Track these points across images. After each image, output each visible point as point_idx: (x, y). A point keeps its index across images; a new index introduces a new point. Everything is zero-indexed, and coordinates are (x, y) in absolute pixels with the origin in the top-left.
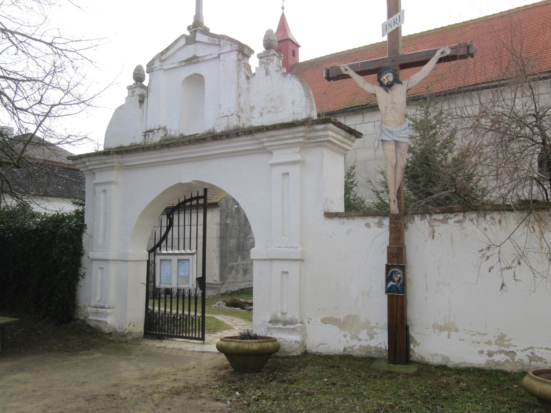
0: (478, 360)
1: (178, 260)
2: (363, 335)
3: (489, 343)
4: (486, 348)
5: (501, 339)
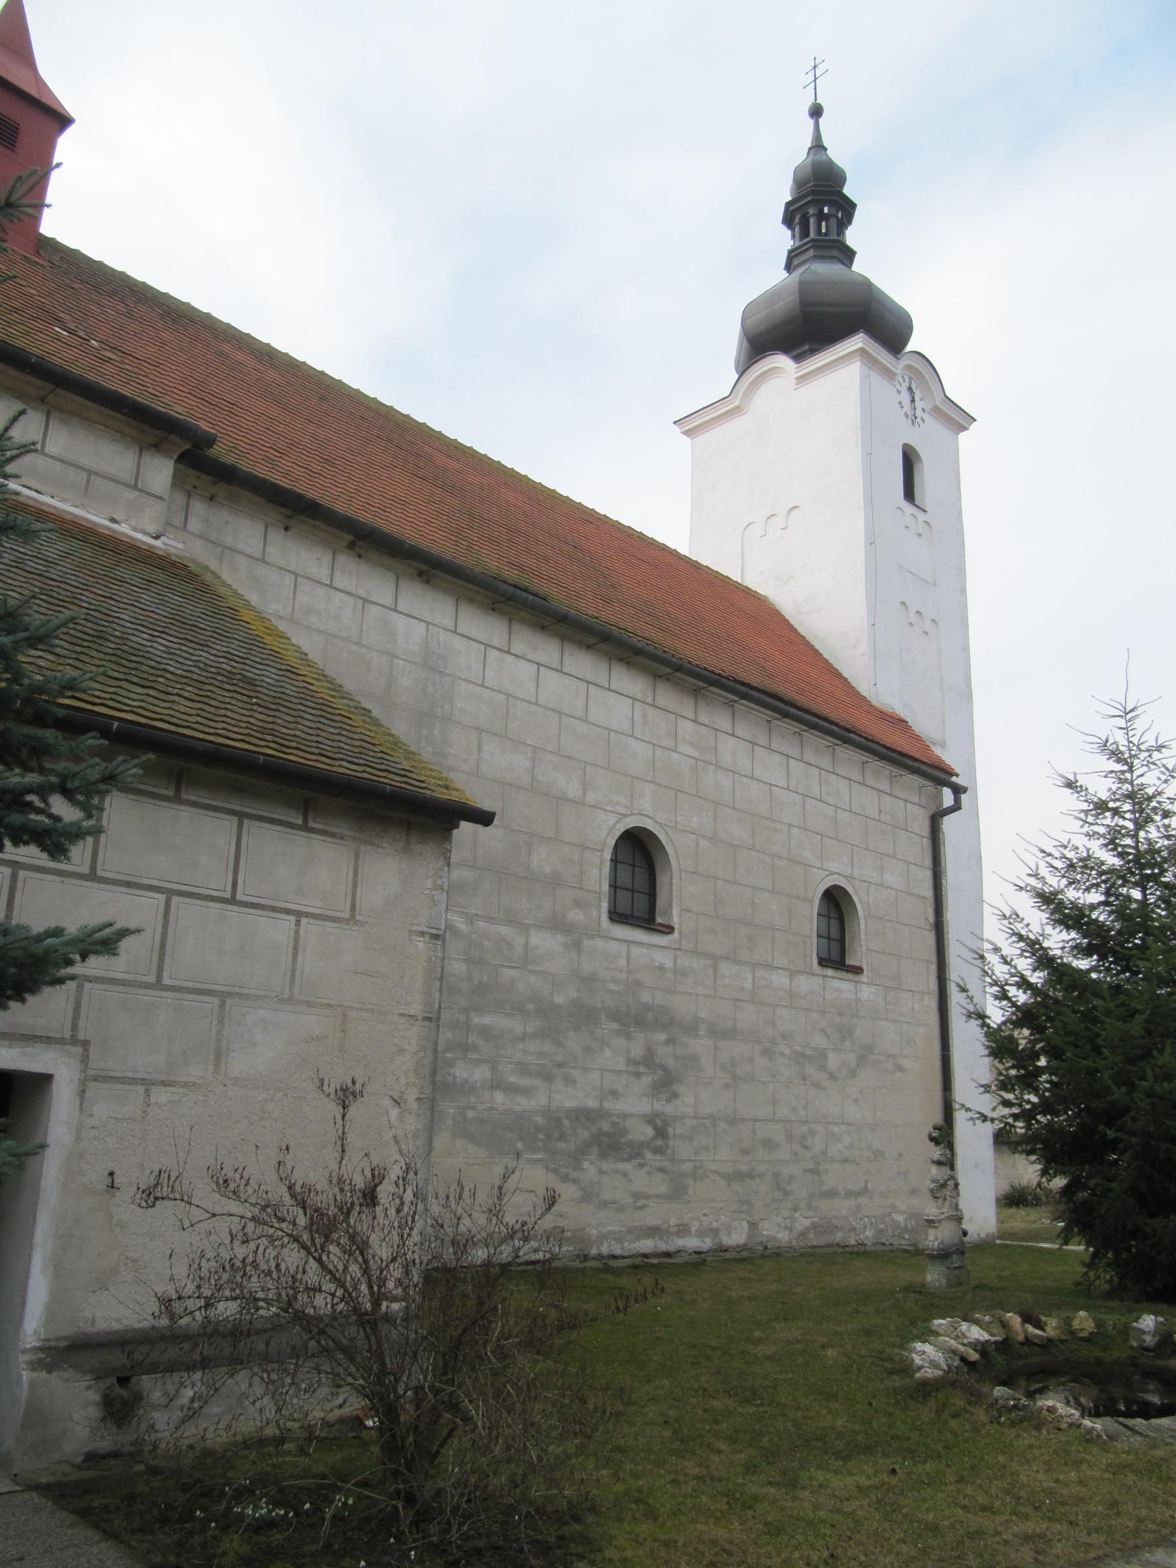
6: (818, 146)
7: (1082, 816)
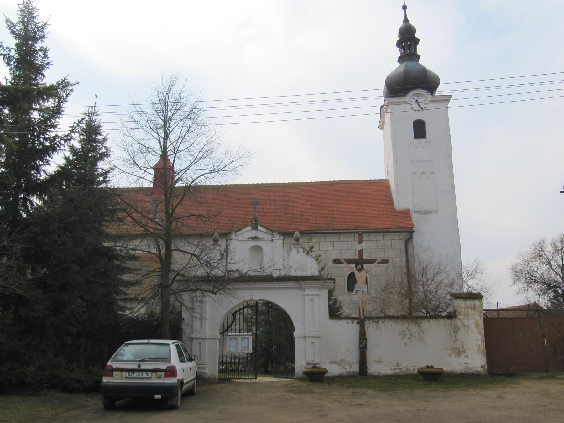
0: (390, 372)
2: (348, 367)
3: (394, 366)
4: (393, 368)
5: (398, 364)
6: (406, 20)
7: (161, 85)
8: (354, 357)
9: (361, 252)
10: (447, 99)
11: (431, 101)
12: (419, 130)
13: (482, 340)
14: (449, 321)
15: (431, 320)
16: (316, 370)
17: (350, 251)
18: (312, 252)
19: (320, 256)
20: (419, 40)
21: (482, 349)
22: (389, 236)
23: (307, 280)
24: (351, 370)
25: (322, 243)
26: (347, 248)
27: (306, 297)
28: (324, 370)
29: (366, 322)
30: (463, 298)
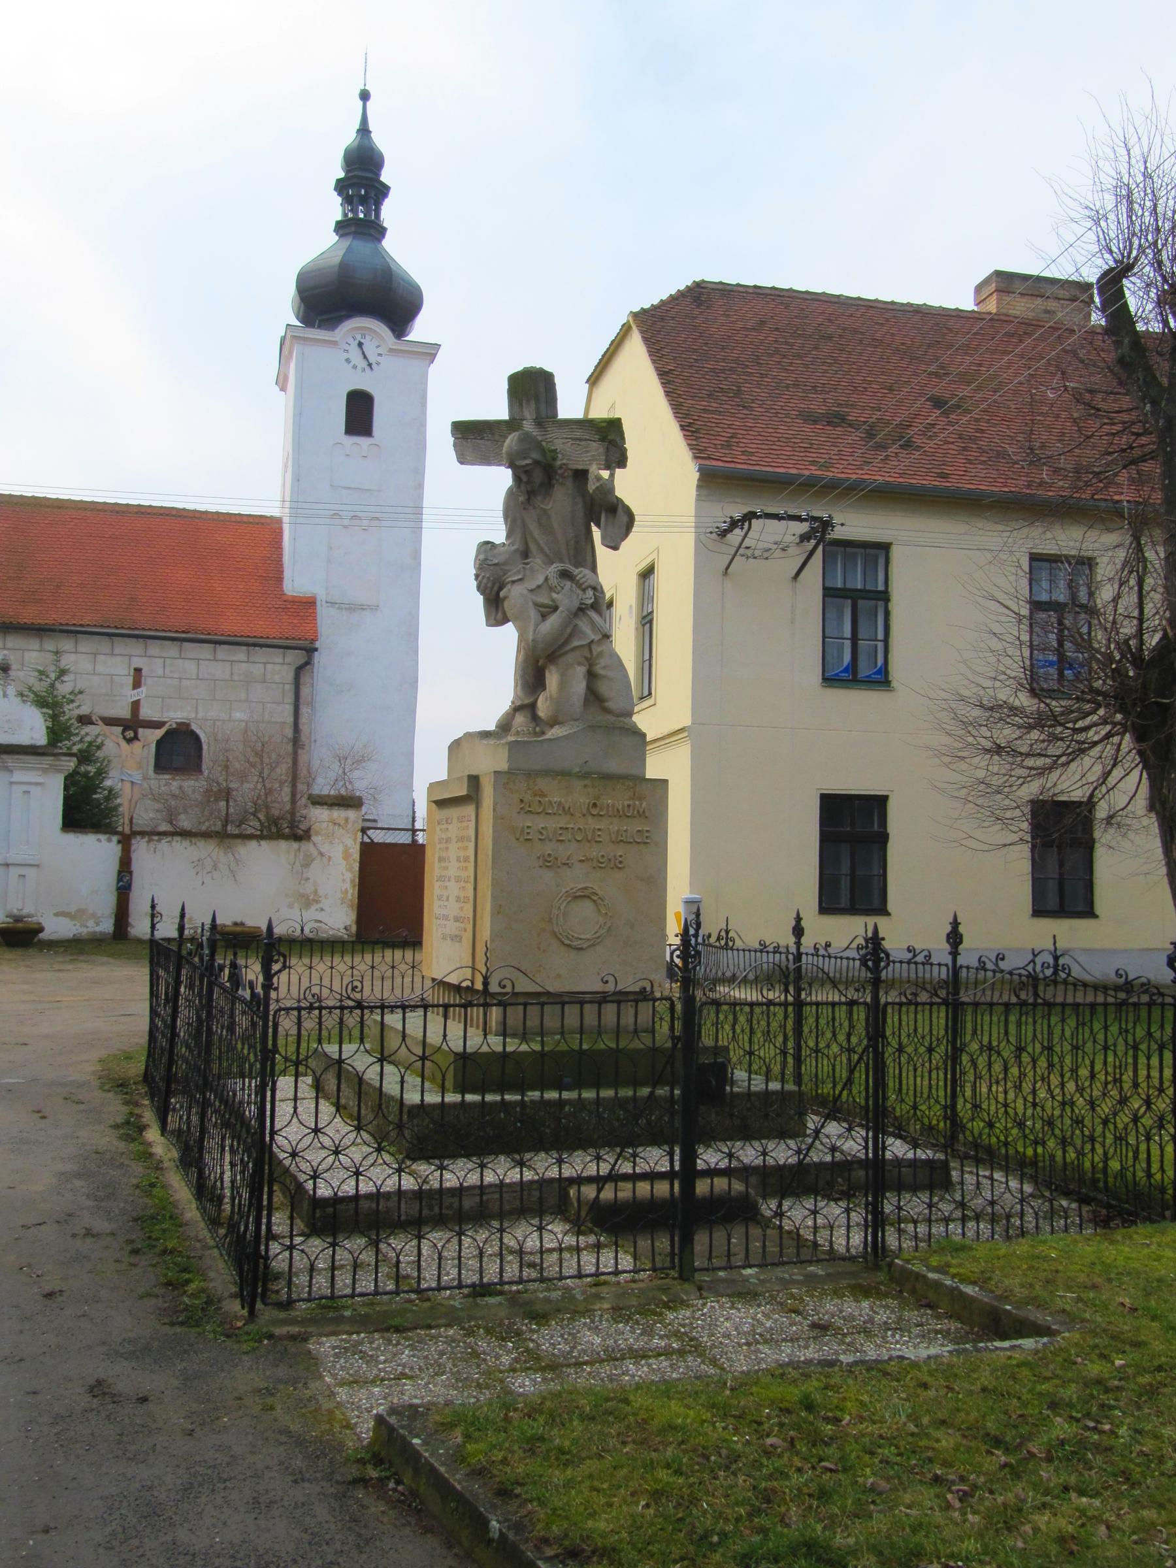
1: (1034, 558)
2: (91, 923)
6: (364, 130)
8: (106, 904)
9: (136, 705)
10: (429, 352)
11: (391, 350)
12: (359, 413)
13: (352, 881)
14: (295, 845)
15: (263, 843)
16: (20, 925)
17: (169, 681)
18: (63, 682)
19: (81, 692)
20: (387, 188)
21: (350, 897)
22: (260, 655)
23: (18, 753)
24: (98, 929)
25: (101, 658)
26: (160, 672)
27: (15, 787)
28: (36, 926)
29: (133, 841)
30: (326, 804)
